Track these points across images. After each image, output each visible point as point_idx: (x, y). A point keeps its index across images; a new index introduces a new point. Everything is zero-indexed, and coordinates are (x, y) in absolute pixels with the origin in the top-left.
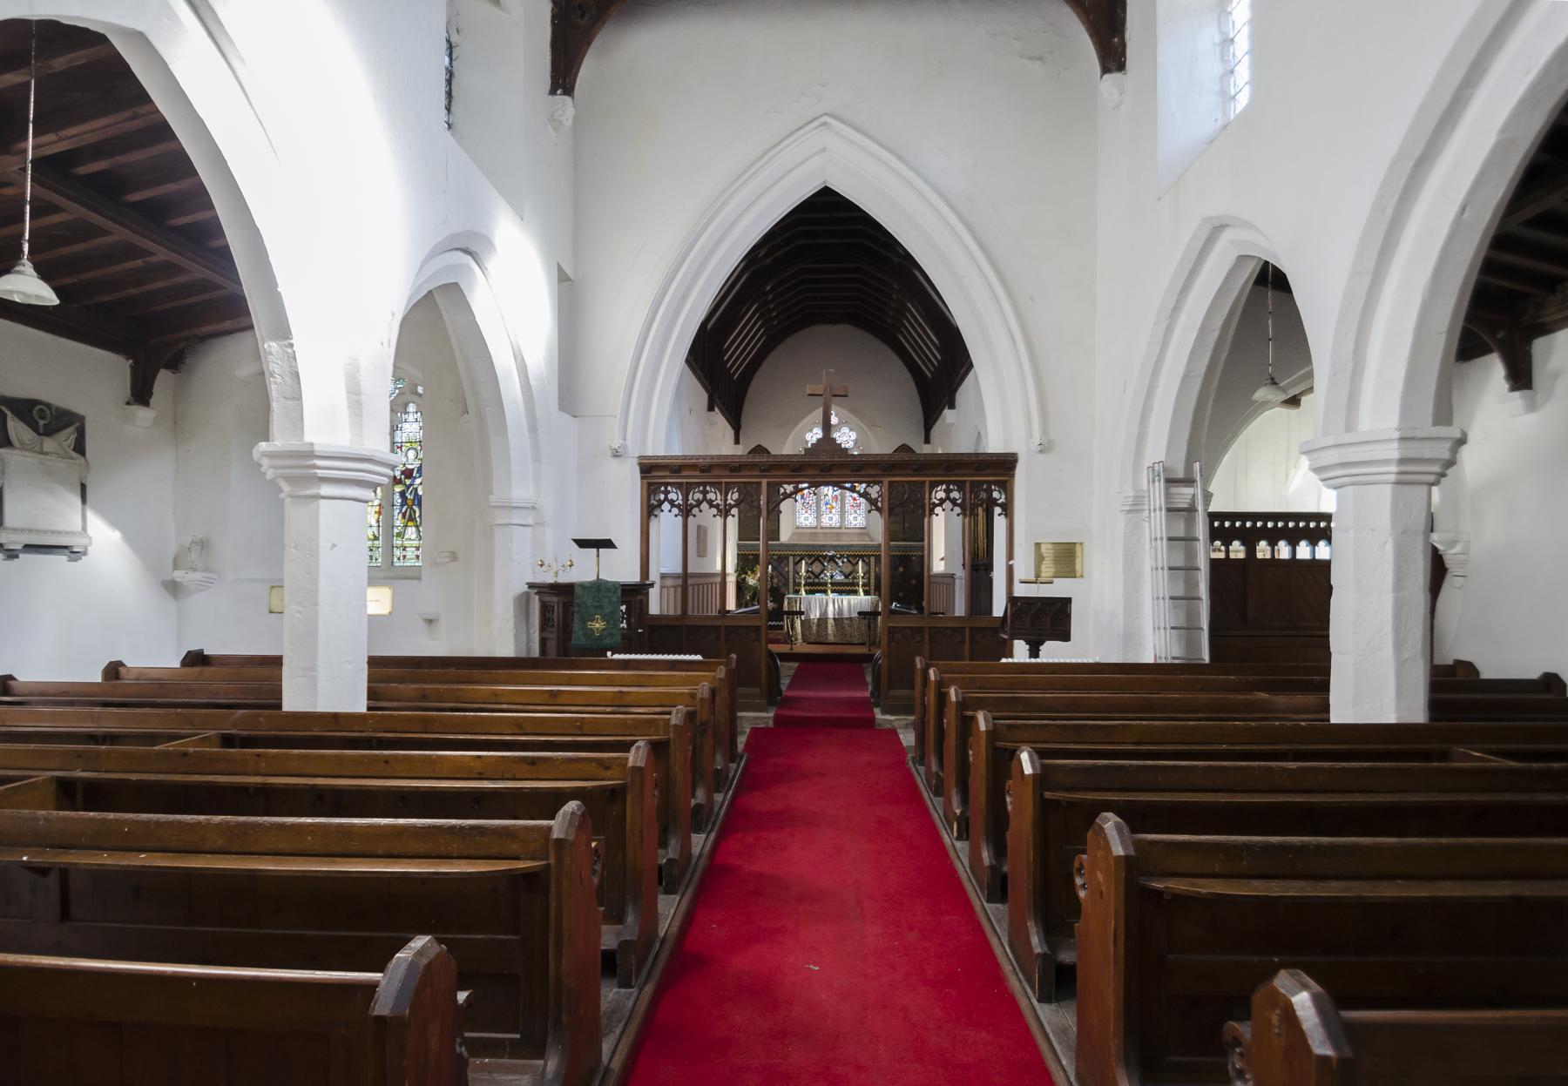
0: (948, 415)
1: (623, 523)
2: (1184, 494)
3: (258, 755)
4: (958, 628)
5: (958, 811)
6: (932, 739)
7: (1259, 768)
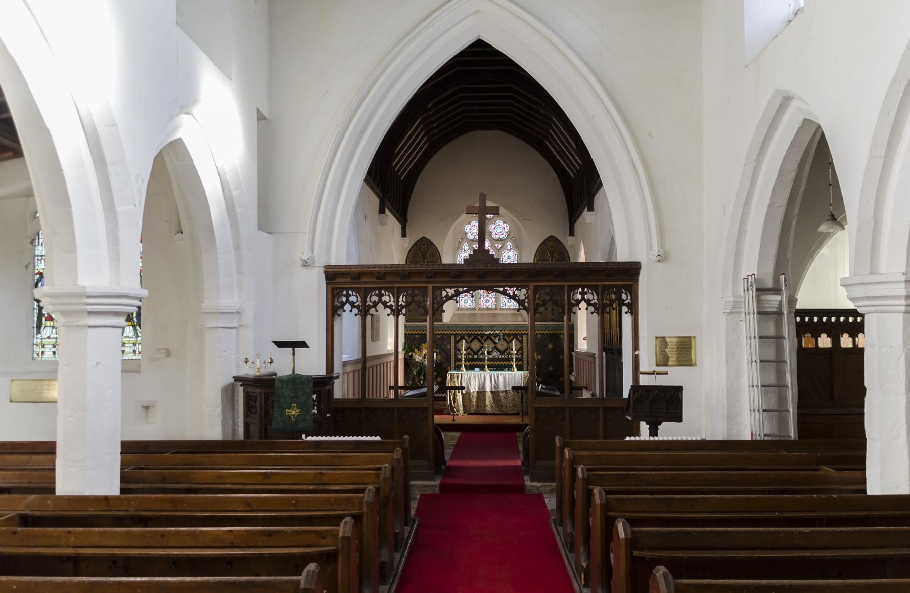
0: (587, 215)
1: (312, 328)
2: (773, 300)
3: (69, 532)
4: (592, 407)
5: (585, 565)
6: (567, 504)
7: (783, 532)
